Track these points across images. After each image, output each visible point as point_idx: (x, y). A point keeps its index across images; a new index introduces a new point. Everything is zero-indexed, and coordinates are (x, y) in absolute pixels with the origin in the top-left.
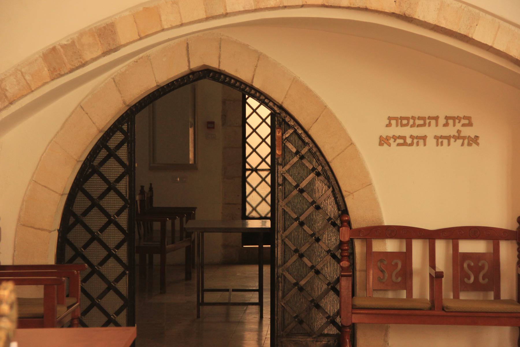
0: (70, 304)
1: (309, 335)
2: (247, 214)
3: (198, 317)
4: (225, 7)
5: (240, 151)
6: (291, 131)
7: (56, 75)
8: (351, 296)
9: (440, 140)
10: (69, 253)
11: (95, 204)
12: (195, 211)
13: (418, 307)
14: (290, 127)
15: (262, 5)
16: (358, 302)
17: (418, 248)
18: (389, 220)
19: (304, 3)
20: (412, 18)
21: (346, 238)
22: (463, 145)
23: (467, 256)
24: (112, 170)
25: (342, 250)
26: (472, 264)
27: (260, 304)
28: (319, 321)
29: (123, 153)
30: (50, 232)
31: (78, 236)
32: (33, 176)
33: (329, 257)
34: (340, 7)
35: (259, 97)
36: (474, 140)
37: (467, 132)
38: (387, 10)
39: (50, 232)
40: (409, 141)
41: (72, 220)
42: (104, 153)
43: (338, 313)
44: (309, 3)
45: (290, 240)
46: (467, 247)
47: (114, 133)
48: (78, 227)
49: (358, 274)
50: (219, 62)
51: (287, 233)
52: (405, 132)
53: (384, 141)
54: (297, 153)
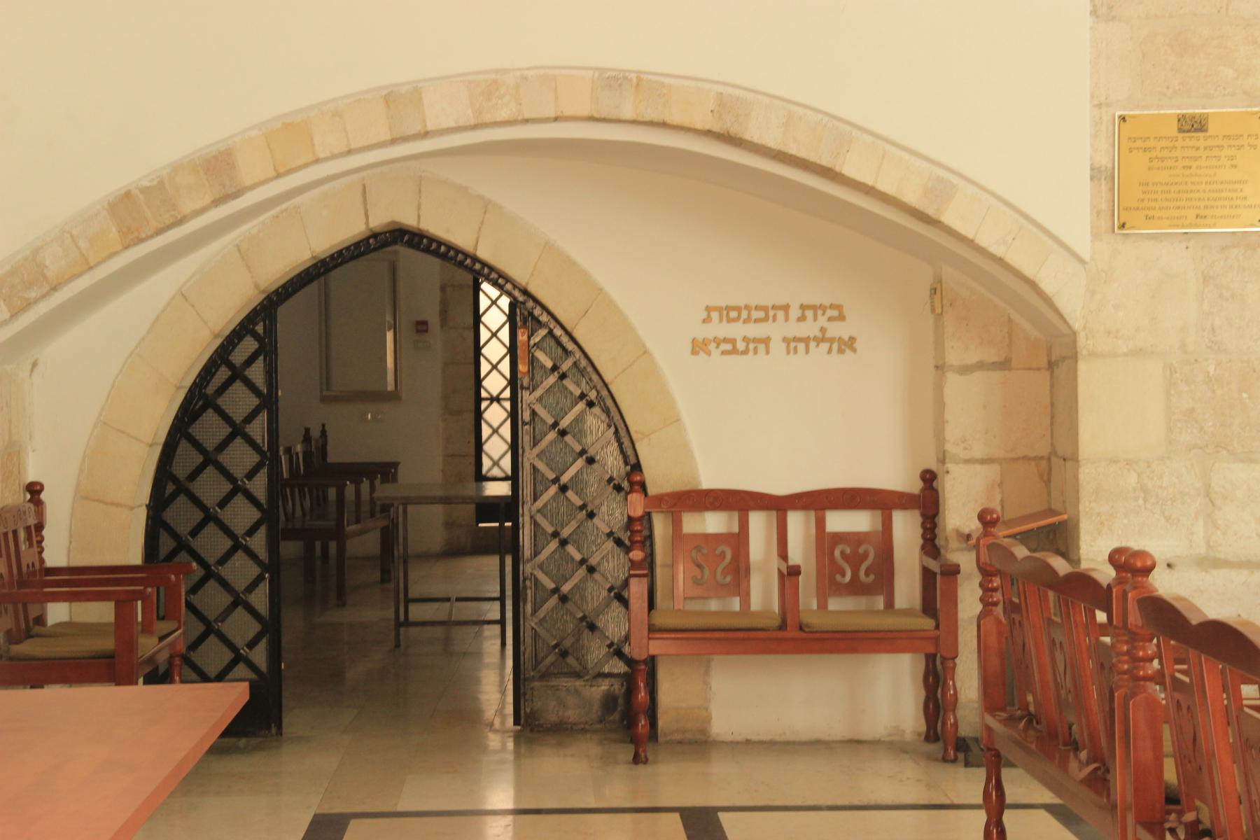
0: (165, 632)
1: (578, 675)
2: (484, 470)
3: (398, 646)
4: (424, 121)
5: (472, 368)
6: (542, 332)
7: (132, 239)
8: (646, 610)
9: (792, 345)
10: (166, 544)
11: (209, 460)
12: (396, 469)
13: (760, 626)
14: (540, 324)
15: (488, 118)
16: (660, 619)
17: (759, 523)
18: (708, 481)
19: (559, 114)
20: (740, 139)
21: (638, 512)
22: (830, 351)
23: (839, 538)
24: (239, 401)
25: (633, 532)
26: (848, 551)
27: (502, 622)
28: (596, 652)
29: (257, 373)
30: (132, 509)
31: (182, 515)
32: (100, 414)
33: (610, 544)
34: (618, 121)
35: (489, 274)
36: (848, 344)
37: (835, 330)
38: (699, 126)
39: (132, 509)
40: (741, 346)
41: (170, 488)
42: (223, 373)
43: (627, 638)
44: (567, 113)
45: (545, 516)
46: (840, 522)
47: (241, 339)
48: (182, 499)
49: (659, 572)
50: (419, 217)
51: (539, 504)
52: (734, 331)
53: (699, 347)
54: (555, 368)
